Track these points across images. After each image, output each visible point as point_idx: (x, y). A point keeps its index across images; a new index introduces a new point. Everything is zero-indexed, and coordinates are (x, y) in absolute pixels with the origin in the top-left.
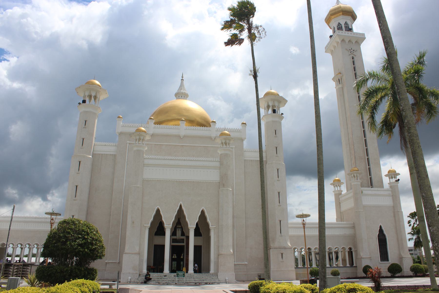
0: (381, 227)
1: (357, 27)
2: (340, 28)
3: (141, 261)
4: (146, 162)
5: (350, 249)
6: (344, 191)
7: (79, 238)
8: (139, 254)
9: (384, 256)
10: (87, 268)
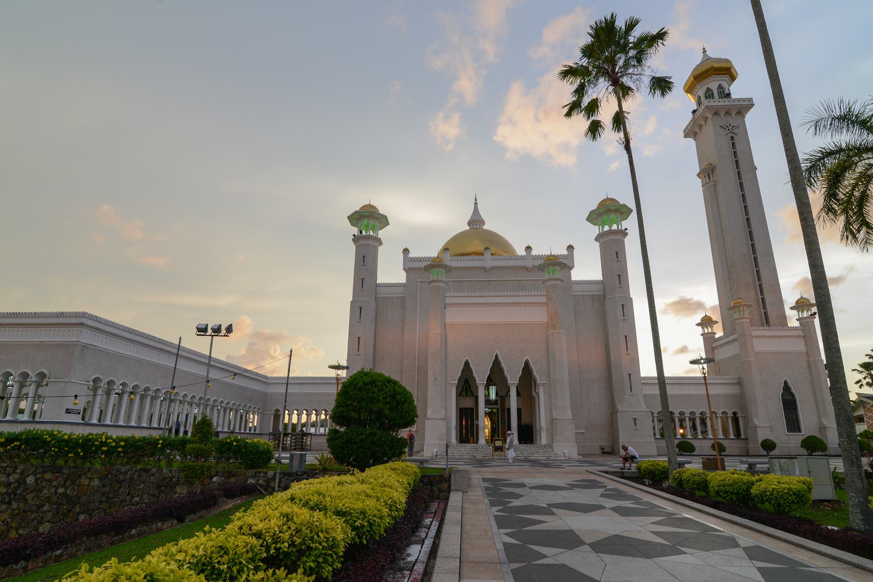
0: (786, 382)
1: (737, 90)
2: (709, 94)
3: (448, 428)
4: (448, 301)
5: (735, 413)
6: (719, 334)
7: (16, 488)
8: (446, 419)
9: (793, 424)
10: (392, 437)
